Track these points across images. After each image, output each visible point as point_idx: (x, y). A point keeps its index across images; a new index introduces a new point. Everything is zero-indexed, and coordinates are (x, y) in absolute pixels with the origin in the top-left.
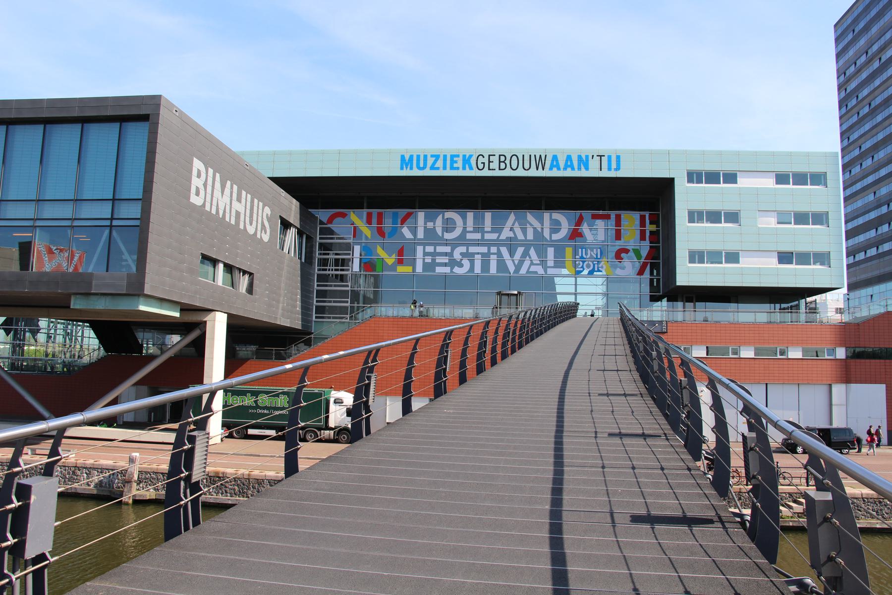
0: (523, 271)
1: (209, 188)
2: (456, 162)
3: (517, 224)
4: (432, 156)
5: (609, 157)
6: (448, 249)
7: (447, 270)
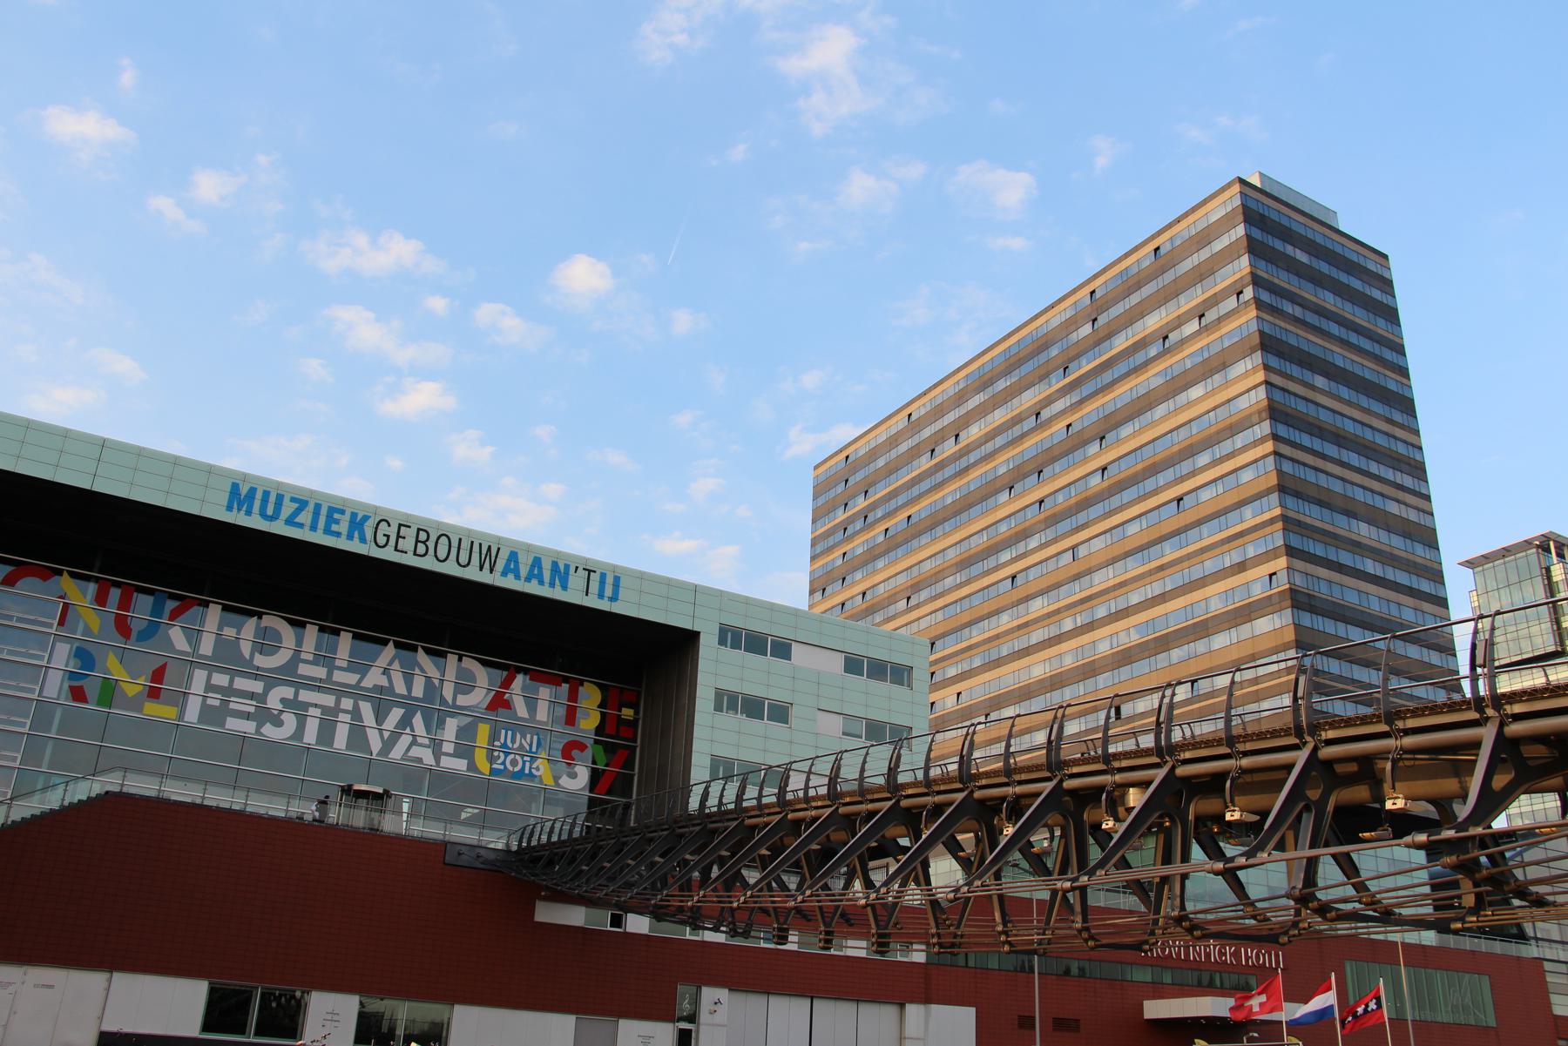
0: (397, 753)
2: (337, 522)
3: (396, 665)
4: (293, 500)
5: (603, 576)
6: (257, 687)
7: (249, 727)
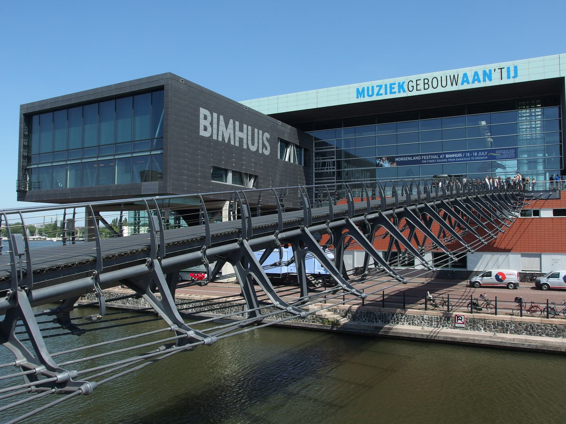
1: (215, 126)
4: (377, 86)
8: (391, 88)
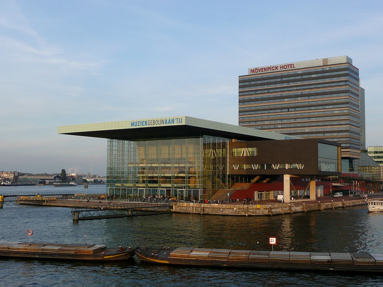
4: (138, 122)
8: (143, 123)
